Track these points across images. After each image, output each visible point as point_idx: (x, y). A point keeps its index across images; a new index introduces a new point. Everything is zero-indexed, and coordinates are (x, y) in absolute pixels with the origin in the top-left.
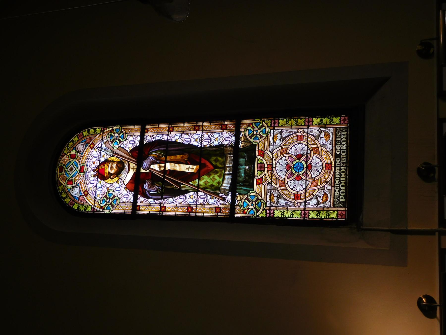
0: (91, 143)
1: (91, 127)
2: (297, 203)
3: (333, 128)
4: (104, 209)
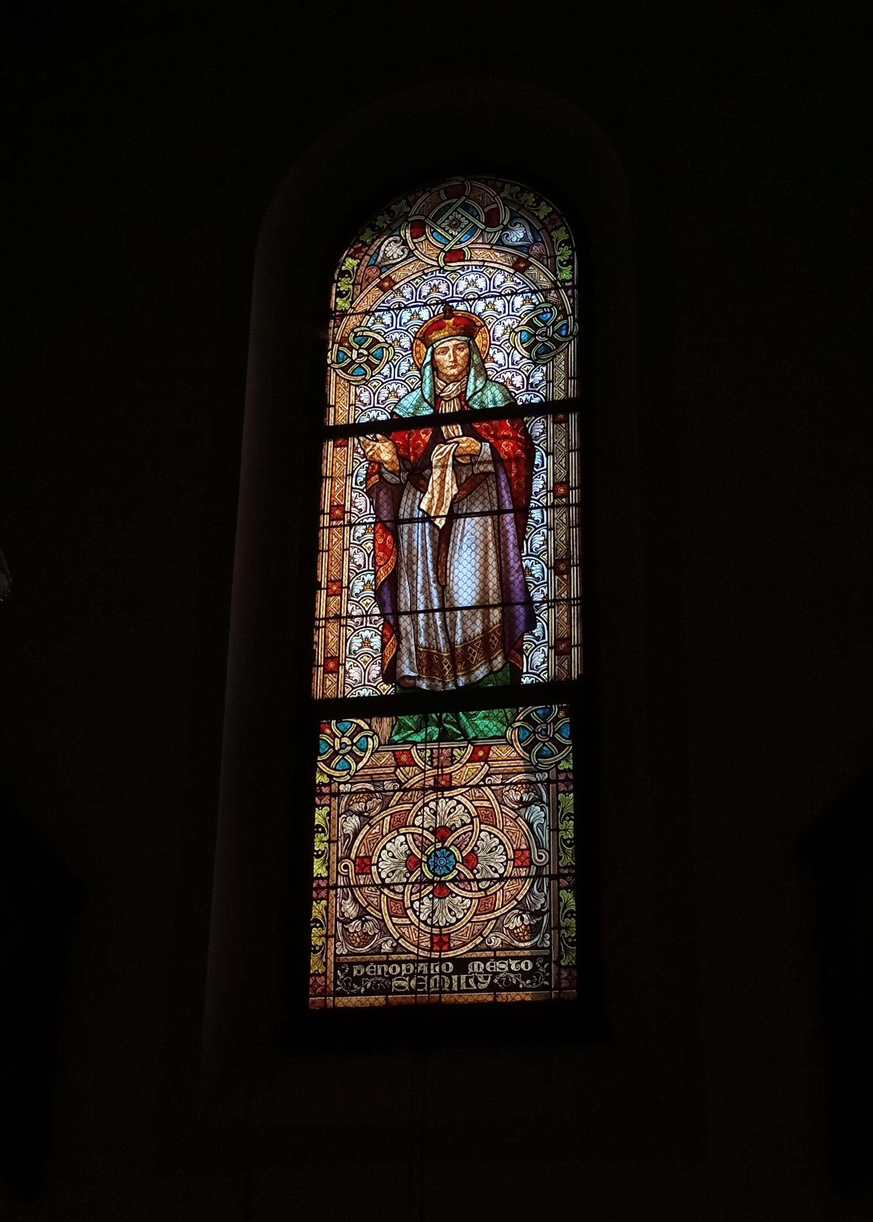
0: (531, 260)
1: (583, 496)
2: (346, 867)
3: (549, 948)
4: (340, 345)
